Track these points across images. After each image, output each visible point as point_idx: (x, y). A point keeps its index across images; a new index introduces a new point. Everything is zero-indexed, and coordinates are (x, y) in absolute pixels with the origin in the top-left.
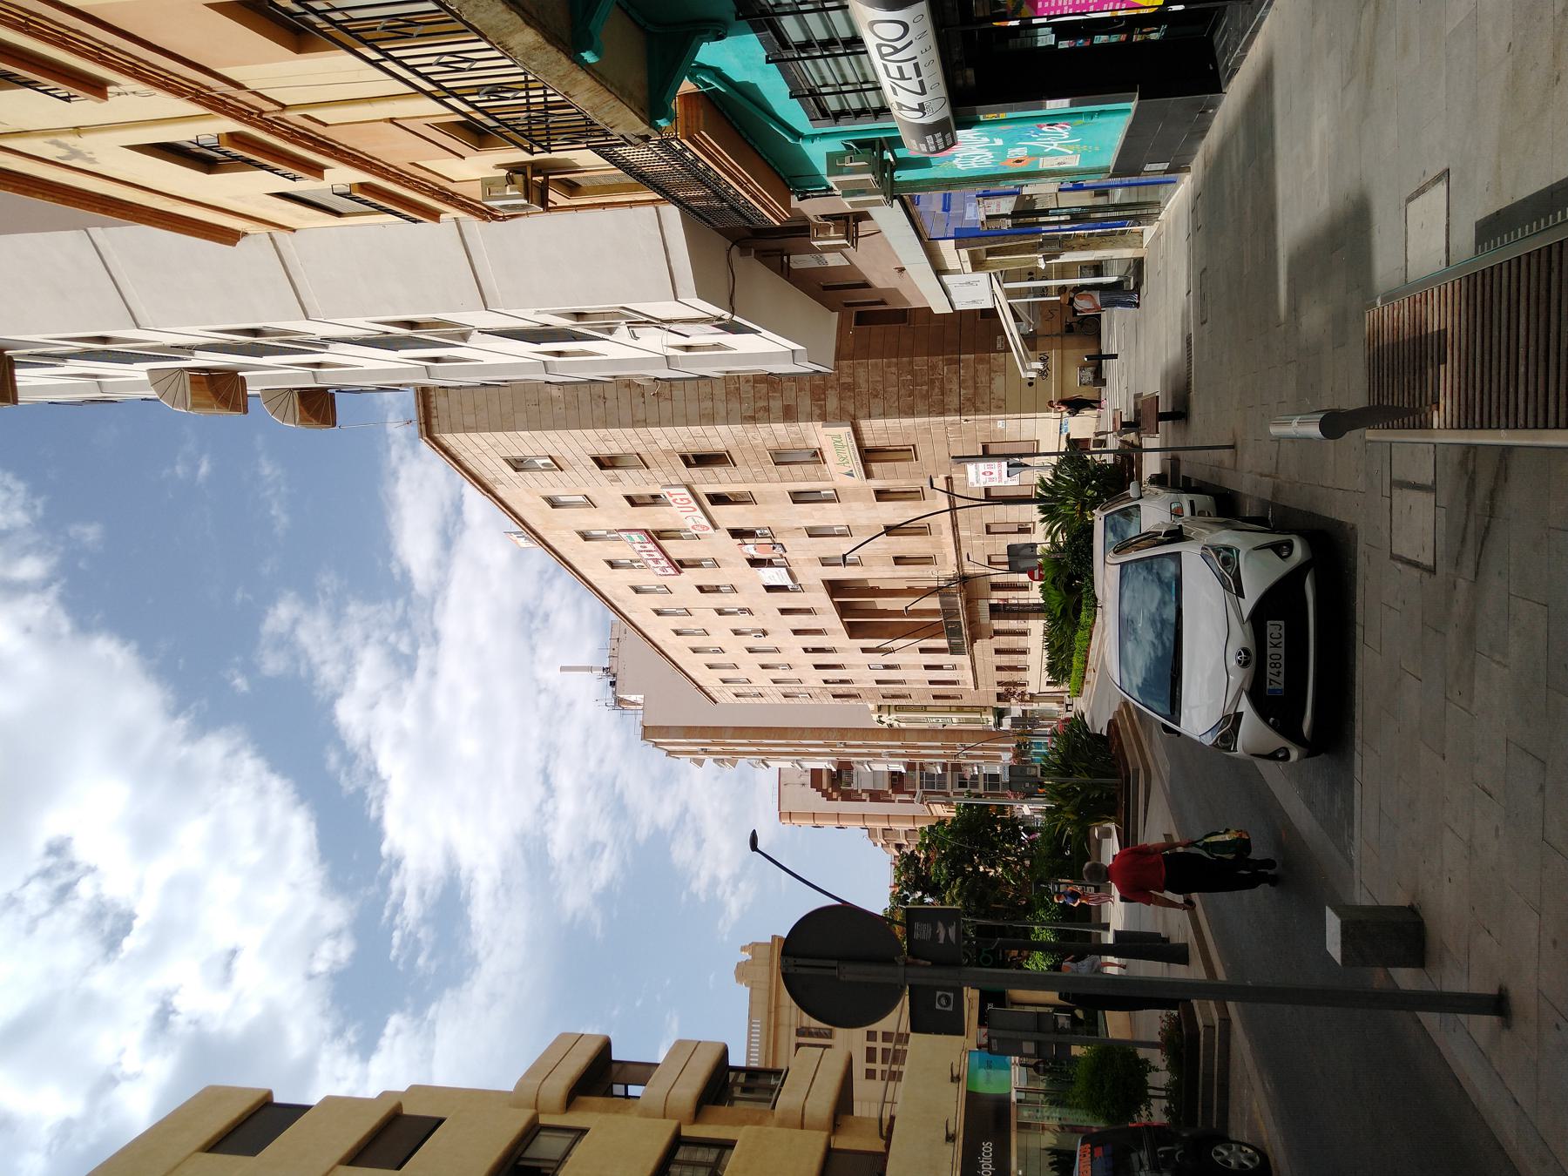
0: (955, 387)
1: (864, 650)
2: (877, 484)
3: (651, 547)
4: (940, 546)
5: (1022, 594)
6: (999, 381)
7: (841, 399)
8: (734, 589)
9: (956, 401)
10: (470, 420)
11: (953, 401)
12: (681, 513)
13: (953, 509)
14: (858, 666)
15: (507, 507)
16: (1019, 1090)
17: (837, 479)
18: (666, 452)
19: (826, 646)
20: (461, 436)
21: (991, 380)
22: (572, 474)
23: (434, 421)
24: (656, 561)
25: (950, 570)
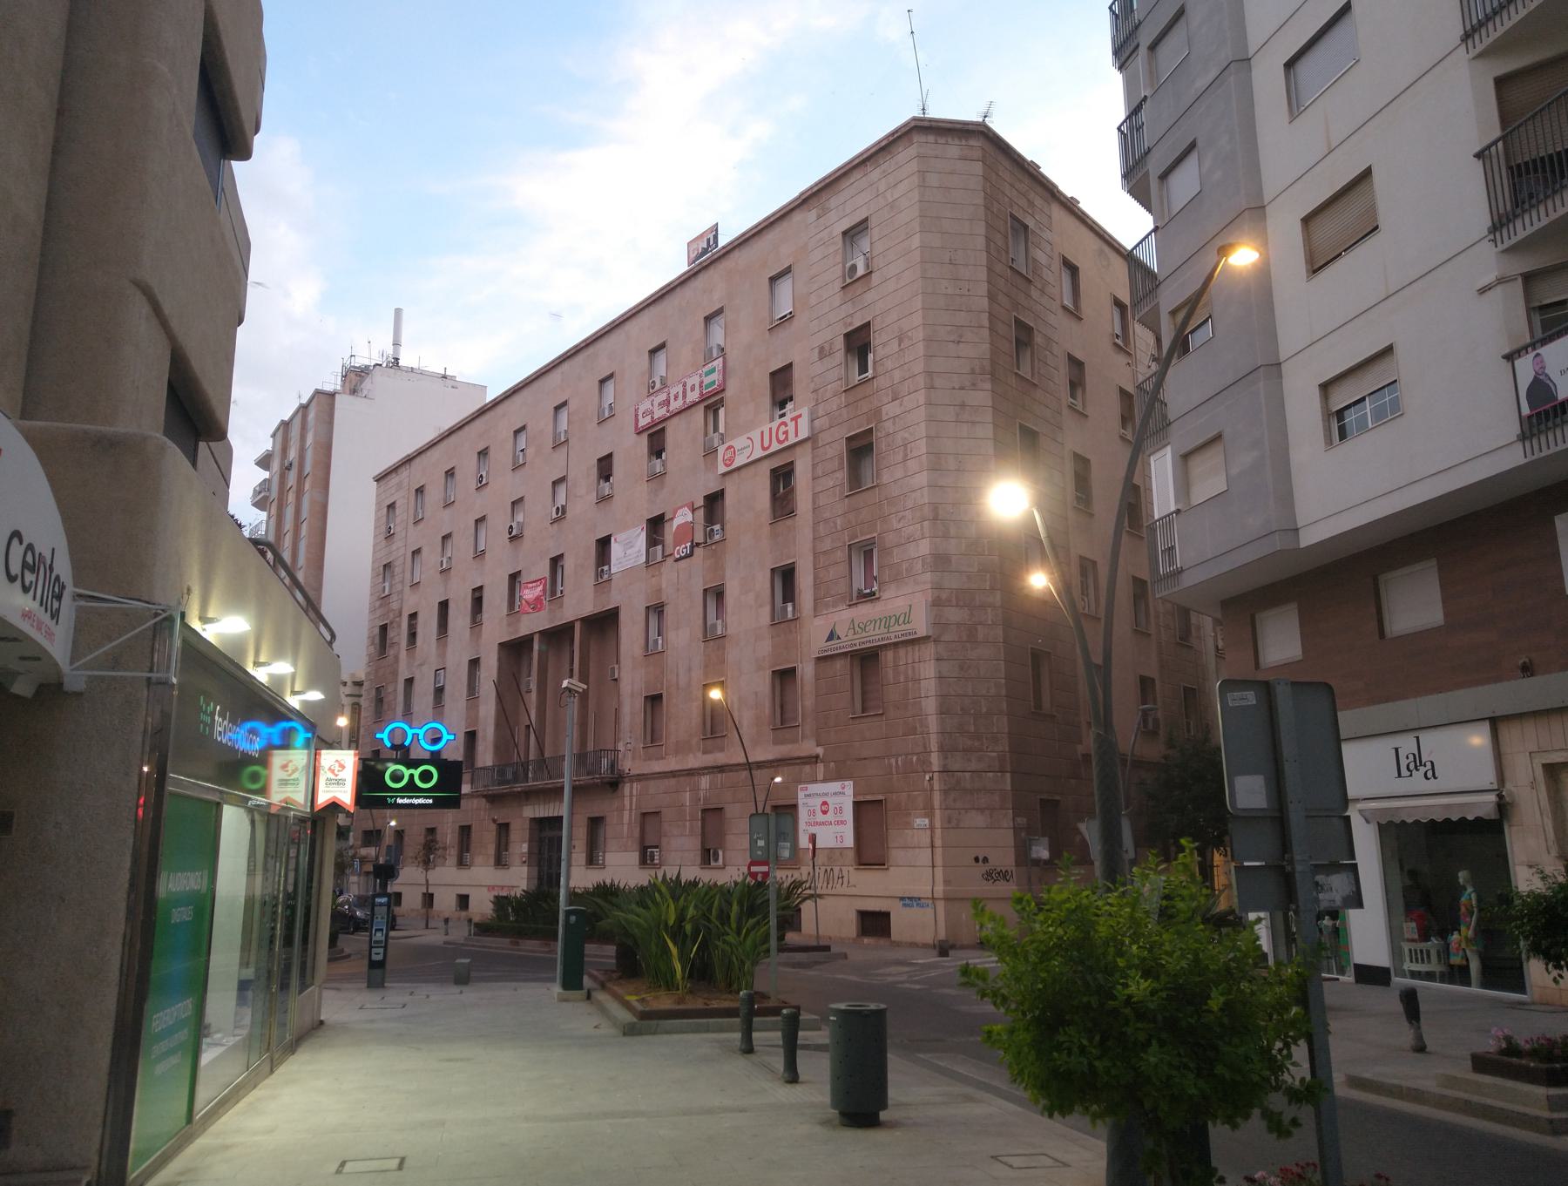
0: (973, 766)
1: (474, 663)
2: (807, 671)
3: (693, 396)
4: (682, 748)
5: (580, 856)
6: (979, 820)
7: (958, 625)
8: (604, 499)
9: (956, 767)
10: (933, 179)
11: (956, 763)
12: (752, 438)
13: (749, 766)
14: (442, 654)
15: (587, 345)
16: (766, 875)
17: (819, 622)
18: (876, 413)
19: (486, 615)
20: (914, 166)
21: (981, 810)
22: (837, 300)
23: (931, 138)
24: (667, 403)
25: (628, 765)
